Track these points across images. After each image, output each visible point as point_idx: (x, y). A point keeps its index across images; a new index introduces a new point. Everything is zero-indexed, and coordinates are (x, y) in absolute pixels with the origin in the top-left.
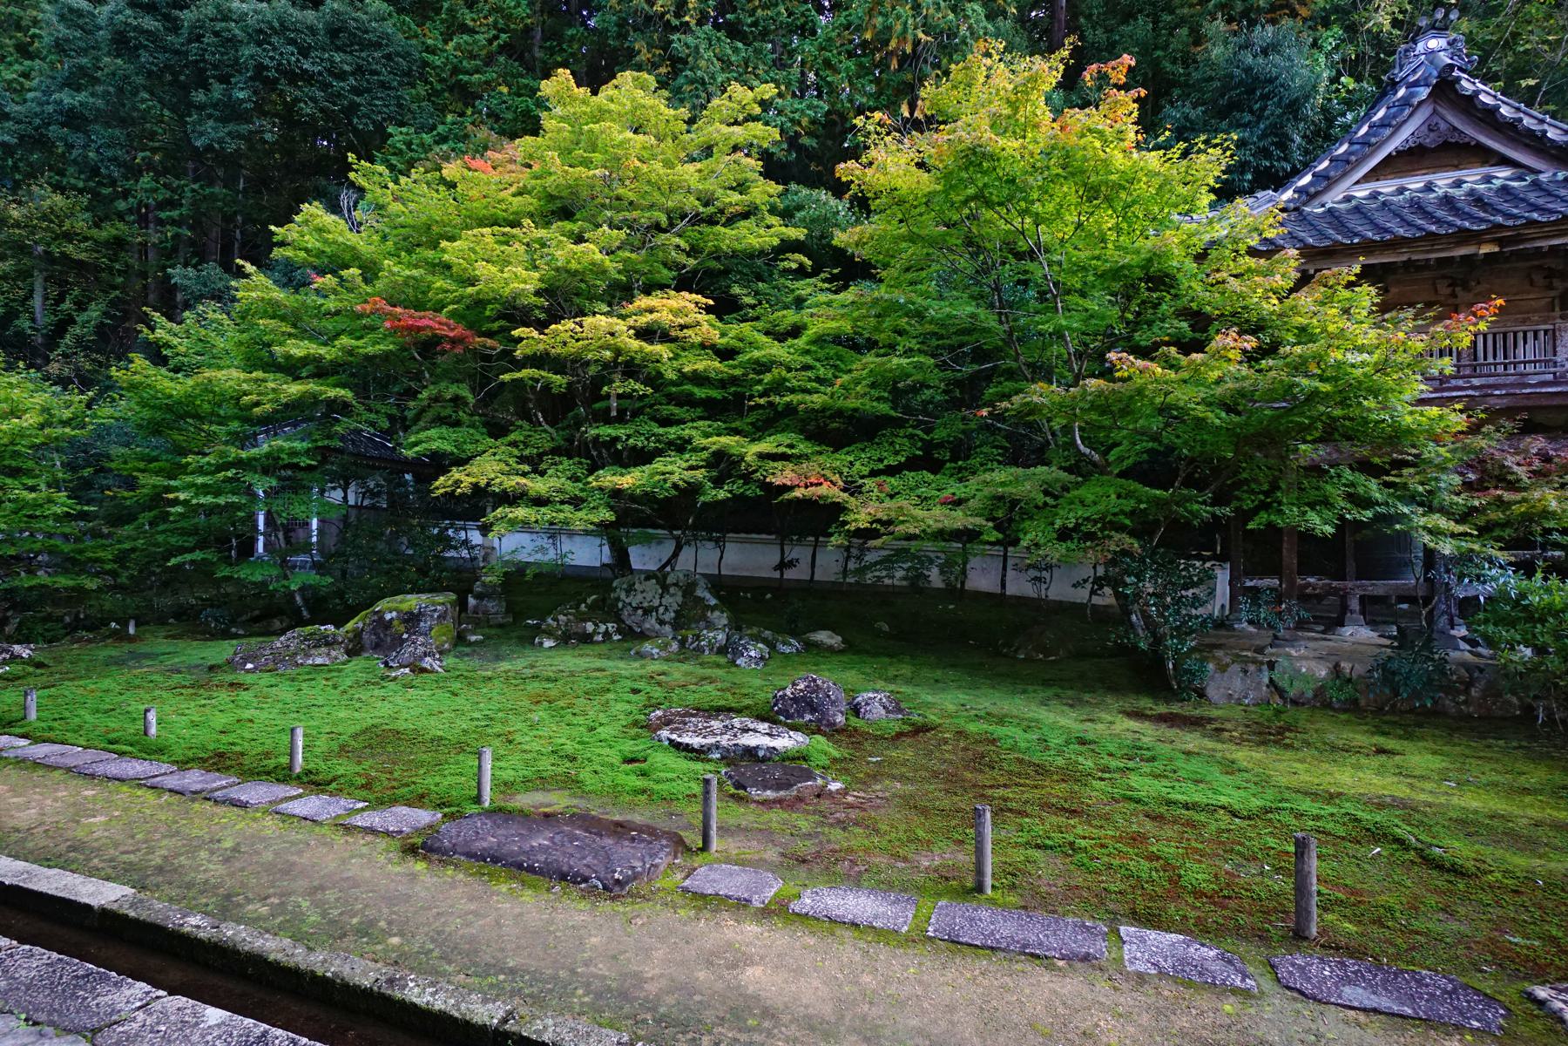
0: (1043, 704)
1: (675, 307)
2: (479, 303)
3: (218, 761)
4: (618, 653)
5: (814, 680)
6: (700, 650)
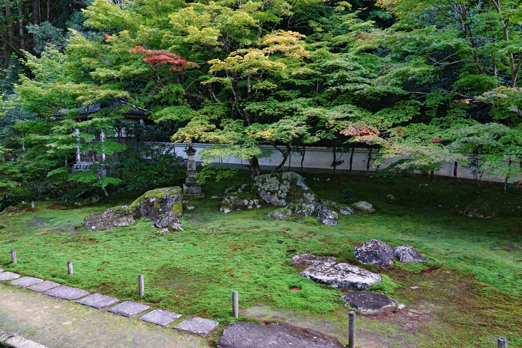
0: (492, 249)
1: (287, 39)
2: (188, 46)
3: (104, 288)
4: (261, 216)
5: (376, 243)
6: (303, 214)
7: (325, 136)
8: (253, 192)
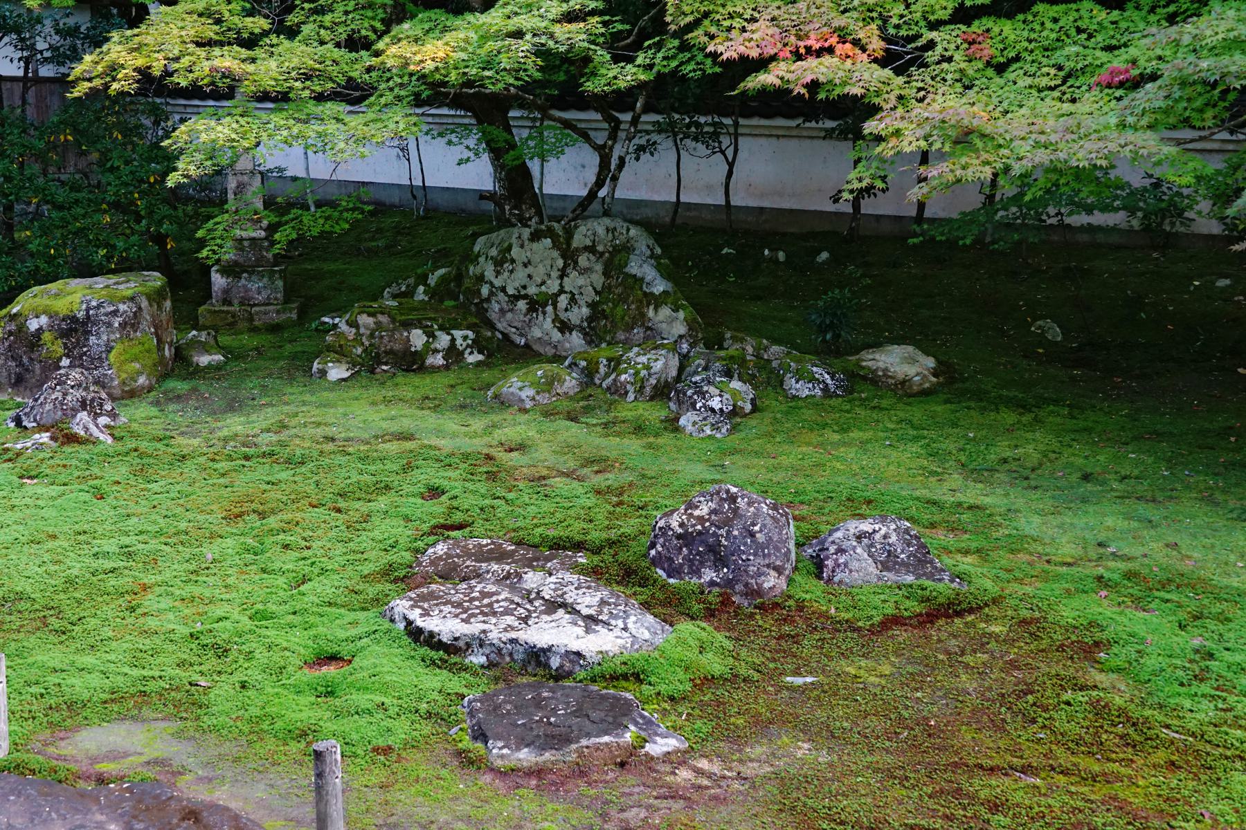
5: (732, 499)
7: (674, 64)
8: (461, 302)
